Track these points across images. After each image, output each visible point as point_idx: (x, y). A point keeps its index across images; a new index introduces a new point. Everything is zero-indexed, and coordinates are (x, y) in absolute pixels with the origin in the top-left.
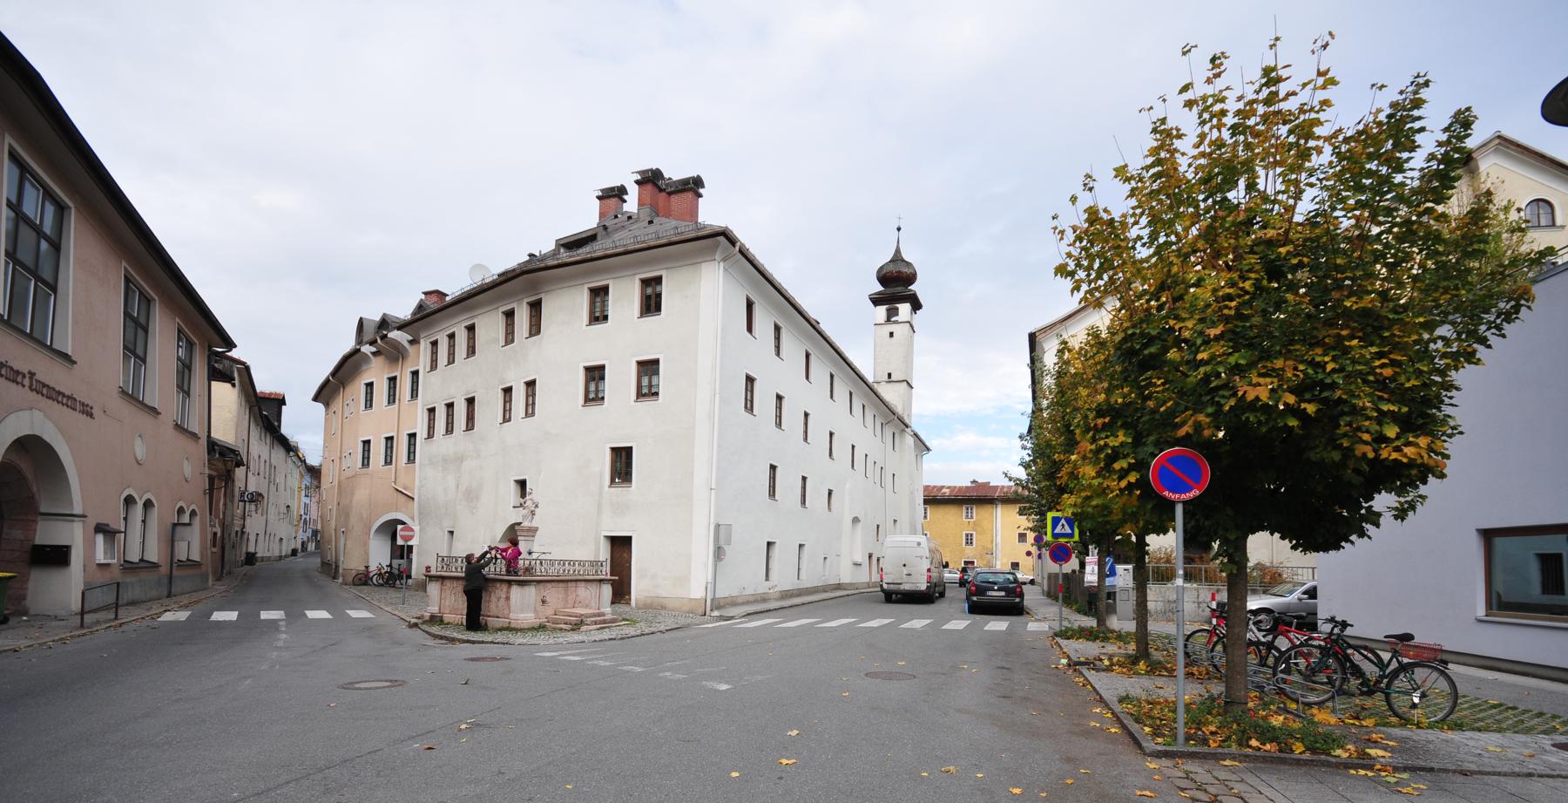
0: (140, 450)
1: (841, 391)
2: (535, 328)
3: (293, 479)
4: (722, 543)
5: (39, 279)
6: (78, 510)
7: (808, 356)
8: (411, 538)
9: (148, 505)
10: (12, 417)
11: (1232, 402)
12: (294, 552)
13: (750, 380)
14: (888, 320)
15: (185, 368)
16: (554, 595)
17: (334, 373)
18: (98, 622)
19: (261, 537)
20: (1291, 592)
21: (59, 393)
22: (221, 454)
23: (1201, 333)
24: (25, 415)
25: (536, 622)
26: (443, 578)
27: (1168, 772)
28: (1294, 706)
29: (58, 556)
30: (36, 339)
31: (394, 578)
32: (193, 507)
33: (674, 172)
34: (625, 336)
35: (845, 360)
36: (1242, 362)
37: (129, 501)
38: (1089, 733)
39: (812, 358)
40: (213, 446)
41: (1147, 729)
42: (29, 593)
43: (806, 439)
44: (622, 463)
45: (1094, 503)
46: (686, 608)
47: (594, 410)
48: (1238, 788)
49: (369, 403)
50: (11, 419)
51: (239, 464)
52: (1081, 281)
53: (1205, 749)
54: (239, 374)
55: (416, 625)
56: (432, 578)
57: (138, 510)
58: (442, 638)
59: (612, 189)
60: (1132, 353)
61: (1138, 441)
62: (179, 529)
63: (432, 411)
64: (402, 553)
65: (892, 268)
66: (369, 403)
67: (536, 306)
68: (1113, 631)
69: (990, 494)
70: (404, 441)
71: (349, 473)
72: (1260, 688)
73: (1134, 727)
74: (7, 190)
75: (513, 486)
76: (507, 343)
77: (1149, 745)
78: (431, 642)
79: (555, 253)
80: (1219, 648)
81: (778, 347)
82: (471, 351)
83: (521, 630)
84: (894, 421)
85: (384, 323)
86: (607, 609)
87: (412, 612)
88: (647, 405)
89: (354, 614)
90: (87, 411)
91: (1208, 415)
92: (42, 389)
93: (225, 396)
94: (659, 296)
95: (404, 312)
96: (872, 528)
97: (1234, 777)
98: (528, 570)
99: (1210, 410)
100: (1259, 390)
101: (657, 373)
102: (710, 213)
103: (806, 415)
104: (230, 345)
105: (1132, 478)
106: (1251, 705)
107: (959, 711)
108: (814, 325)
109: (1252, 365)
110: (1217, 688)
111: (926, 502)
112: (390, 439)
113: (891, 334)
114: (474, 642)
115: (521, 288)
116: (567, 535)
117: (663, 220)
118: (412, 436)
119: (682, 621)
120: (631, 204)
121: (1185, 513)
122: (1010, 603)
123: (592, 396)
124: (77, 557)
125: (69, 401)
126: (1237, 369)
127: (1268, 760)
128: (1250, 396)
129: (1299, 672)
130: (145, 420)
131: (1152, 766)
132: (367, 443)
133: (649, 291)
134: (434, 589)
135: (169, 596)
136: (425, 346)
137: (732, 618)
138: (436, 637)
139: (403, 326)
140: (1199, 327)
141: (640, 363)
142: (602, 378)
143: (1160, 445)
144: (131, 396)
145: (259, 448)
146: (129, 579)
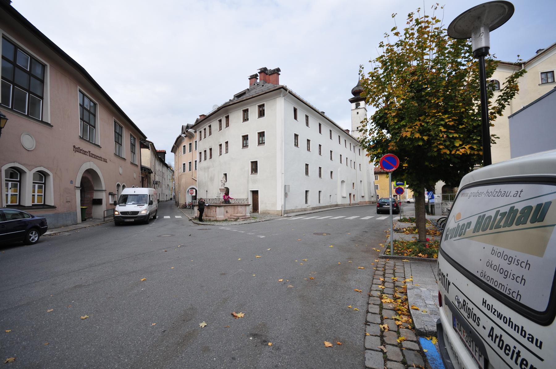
0: (121, 171)
1: (335, 136)
2: (227, 125)
4: (287, 192)
5: (90, 125)
6: (104, 189)
12: (171, 199)
13: (296, 136)
14: (357, 108)
15: (133, 145)
17: (175, 143)
24: (88, 163)
25: (224, 219)
33: (271, 67)
34: (255, 125)
35: (335, 125)
37: (118, 185)
39: (322, 126)
40: (143, 169)
43: (320, 154)
44: (254, 166)
47: (245, 149)
50: (84, 165)
54: (144, 143)
55: (191, 220)
63: (200, 153)
65: (357, 89)
66: (184, 152)
67: (227, 117)
71: (180, 174)
74: (79, 101)
75: (223, 175)
78: (193, 225)
79: (234, 99)
82: (210, 134)
83: (220, 221)
85: (188, 127)
86: (248, 215)
88: (261, 147)
89: (176, 217)
90: (105, 161)
93: (146, 154)
94: (264, 110)
95: (193, 122)
108: (322, 114)
111: (375, 173)
112: (190, 163)
113: (358, 113)
115: (223, 112)
116: (240, 193)
117: (267, 84)
118: (196, 161)
119: (273, 218)
124: (104, 202)
130: (121, 162)
132: (184, 164)
133: (261, 109)
136: (198, 133)
139: (192, 127)
141: (258, 133)
142: (248, 139)
145: (158, 167)
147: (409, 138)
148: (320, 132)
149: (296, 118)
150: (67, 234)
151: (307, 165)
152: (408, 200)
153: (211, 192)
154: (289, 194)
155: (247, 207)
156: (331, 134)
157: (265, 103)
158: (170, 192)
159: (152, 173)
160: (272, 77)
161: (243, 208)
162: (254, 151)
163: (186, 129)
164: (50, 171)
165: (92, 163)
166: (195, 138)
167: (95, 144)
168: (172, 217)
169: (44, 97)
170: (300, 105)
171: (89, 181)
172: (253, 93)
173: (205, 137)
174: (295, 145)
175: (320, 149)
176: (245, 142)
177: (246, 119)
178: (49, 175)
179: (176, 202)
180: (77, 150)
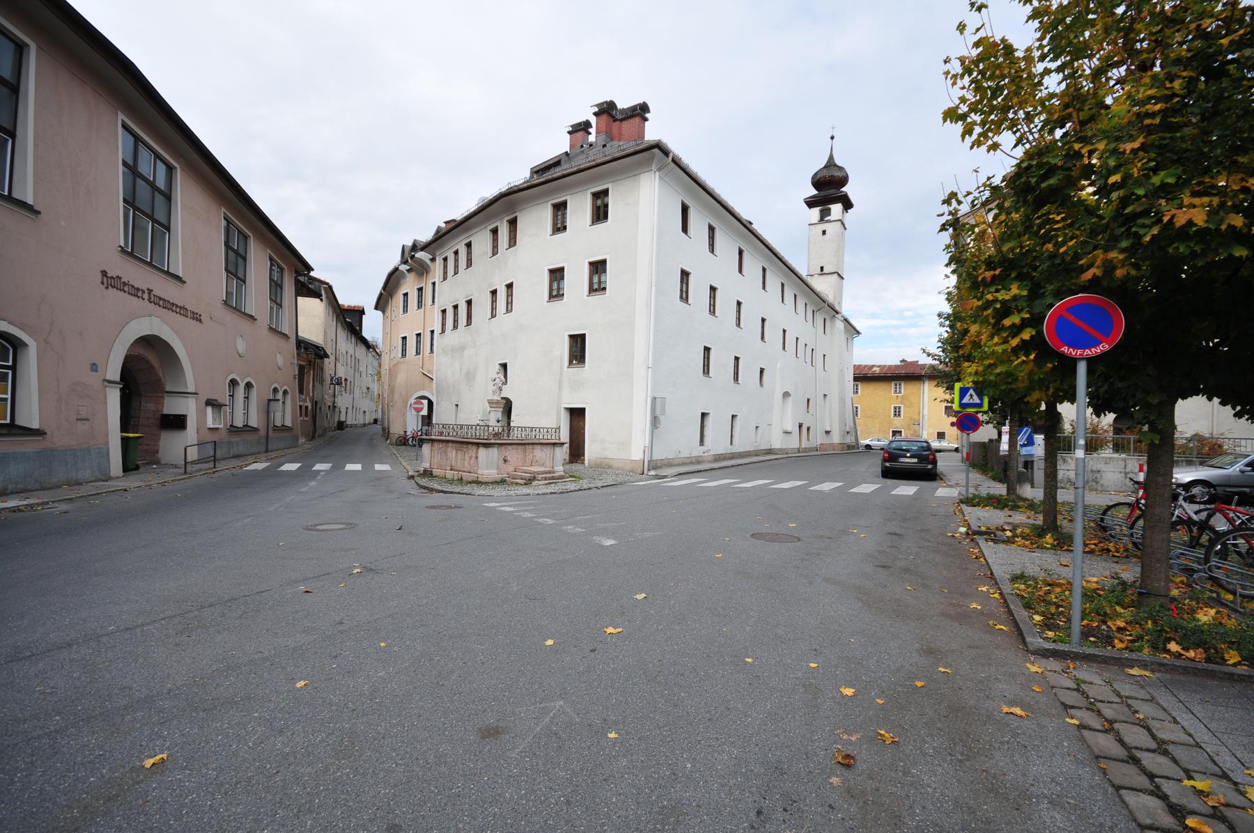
0: (241, 346)
1: (774, 282)
2: (513, 241)
4: (658, 413)
5: (154, 221)
6: (191, 389)
7: (741, 252)
9: (249, 386)
10: (135, 322)
11: (1155, 231)
12: (376, 421)
13: (685, 275)
14: (822, 220)
17: (384, 288)
18: (200, 470)
20: (1232, 464)
23: (1115, 152)
24: (145, 321)
27: (1054, 679)
28: (1230, 597)
29: (178, 423)
33: (623, 103)
34: (582, 240)
35: (776, 255)
36: (1171, 180)
38: (964, 617)
40: (302, 345)
41: (1037, 618)
43: (738, 324)
44: (578, 345)
45: (998, 371)
46: (628, 468)
47: (557, 304)
48: (1145, 710)
49: (405, 309)
50: (133, 324)
52: (974, 123)
53: (1108, 651)
54: (310, 287)
55: (412, 477)
57: (240, 391)
58: (425, 488)
59: (579, 124)
60: (1028, 189)
61: (1035, 293)
62: (272, 403)
63: (444, 311)
65: (825, 173)
66: (405, 309)
67: (513, 223)
68: (1026, 500)
69: (918, 371)
70: (429, 334)
71: (394, 362)
72: (1189, 571)
73: (1021, 614)
77: (1035, 641)
78: (416, 491)
79: (532, 177)
80: (1141, 523)
82: (469, 263)
83: (486, 483)
84: (825, 309)
85: (415, 247)
86: (560, 469)
88: (597, 298)
89: (378, 467)
90: (197, 318)
91: (1123, 251)
94: (606, 206)
95: (426, 236)
96: (788, 396)
97: (1142, 694)
99: (1124, 244)
100: (1192, 212)
102: (653, 131)
103: (739, 304)
104: (310, 269)
105: (1026, 335)
106: (1175, 592)
107: (826, 580)
108: (747, 226)
109: (1181, 185)
110: (1130, 573)
111: (856, 379)
112: (418, 335)
113: (824, 232)
115: (502, 209)
116: (539, 412)
118: (432, 332)
121: (1090, 372)
122: (923, 468)
123: (555, 293)
124: (191, 423)
125: (182, 310)
126: (1165, 191)
127: (1190, 671)
128: (1181, 220)
129: (1239, 553)
130: (244, 324)
131: (1034, 669)
132: (404, 338)
133: (599, 202)
135: (267, 451)
136: (439, 261)
137: (666, 477)
139: (425, 247)
140: (1112, 146)
141: (591, 264)
142: (562, 278)
143: (1059, 295)
145: (345, 344)
146: (235, 439)
147: (1203, 232)
148: (740, 271)
149: (685, 229)
150: (64, 507)
151: (707, 350)
153: (469, 408)
154: (661, 418)
155: (558, 450)
156: (764, 277)
157: (609, 186)
158: (373, 406)
159: (327, 356)
160: (629, 127)
161: (548, 450)
163: (410, 254)
164: (30, 334)
165: (156, 321)
166: (430, 275)
167: (281, 333)
168: (368, 466)
169: (19, 132)
170: (699, 199)
171: (152, 367)
172: (581, 162)
173: (456, 273)
174: (681, 297)
175: (739, 311)
176: (555, 286)
178: (25, 345)
179: (384, 429)
180: (111, 282)
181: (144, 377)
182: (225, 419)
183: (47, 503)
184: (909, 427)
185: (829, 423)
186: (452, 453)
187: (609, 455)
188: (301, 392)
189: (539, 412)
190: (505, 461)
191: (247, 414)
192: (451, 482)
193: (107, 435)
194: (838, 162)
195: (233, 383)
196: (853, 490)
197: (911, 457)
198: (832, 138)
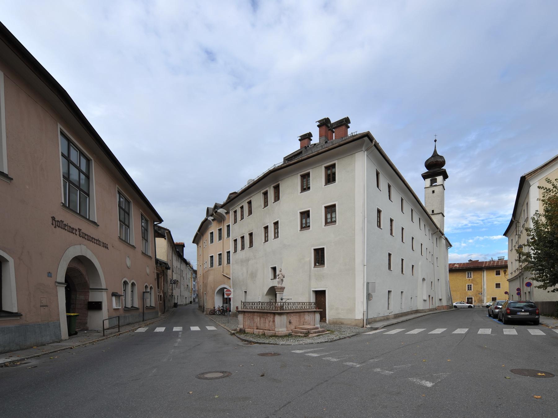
0: (129, 263)
3: (189, 274)
4: (370, 292)
5: (81, 190)
6: (104, 287)
8: (230, 294)
9: (133, 284)
12: (191, 302)
13: (379, 211)
14: (431, 185)
15: (145, 231)
16: (294, 319)
17: (199, 230)
18: (111, 333)
19: (179, 297)
21: (93, 238)
22: (160, 264)
24: (78, 247)
26: (244, 312)
29: (97, 306)
30: (82, 215)
31: (225, 312)
32: (151, 285)
34: (320, 194)
40: (157, 261)
42: (88, 321)
44: (319, 256)
46: (354, 324)
47: (306, 232)
51: (168, 268)
54: (164, 233)
55: (234, 334)
56: (240, 312)
57: (129, 287)
58: (245, 341)
62: (145, 294)
63: (236, 241)
64: (227, 301)
65: (433, 159)
66: (212, 241)
67: (277, 188)
71: (206, 270)
75: (270, 270)
76: (265, 207)
78: (241, 343)
81: (390, 196)
82: (250, 212)
84: (437, 232)
85: (216, 207)
87: (231, 327)
88: (330, 227)
89: (209, 328)
90: (105, 246)
92: (84, 236)
93: (161, 244)
94: (334, 174)
95: (222, 200)
98: (282, 307)
101: (335, 211)
104: (161, 221)
112: (220, 255)
113: (433, 192)
114: (260, 343)
115: (269, 183)
116: (297, 293)
118: (229, 252)
119: (355, 331)
120: (315, 140)
123: (304, 226)
124: (105, 306)
125: (97, 242)
132: (212, 257)
133: (329, 172)
134: (240, 317)
135: (143, 321)
136: (232, 213)
138: (243, 340)
139: (222, 206)
141: (326, 207)
144: (125, 241)
145: (176, 263)
150: (34, 362)
152: (488, 304)
157: (336, 162)
162: (319, 233)
165: (84, 247)
171: (82, 274)
177: (305, 188)
179: (200, 307)
180: (58, 224)
181: (78, 279)
182: (122, 303)
183: (24, 359)
184: (476, 295)
185: (441, 296)
186: (257, 319)
187: (341, 316)
188: (158, 288)
189: (297, 293)
190: (290, 323)
191: (133, 300)
192: (258, 336)
193: (59, 315)
194: (439, 153)
195: (125, 283)
196: (445, 329)
197: (525, 311)
198: (435, 141)
